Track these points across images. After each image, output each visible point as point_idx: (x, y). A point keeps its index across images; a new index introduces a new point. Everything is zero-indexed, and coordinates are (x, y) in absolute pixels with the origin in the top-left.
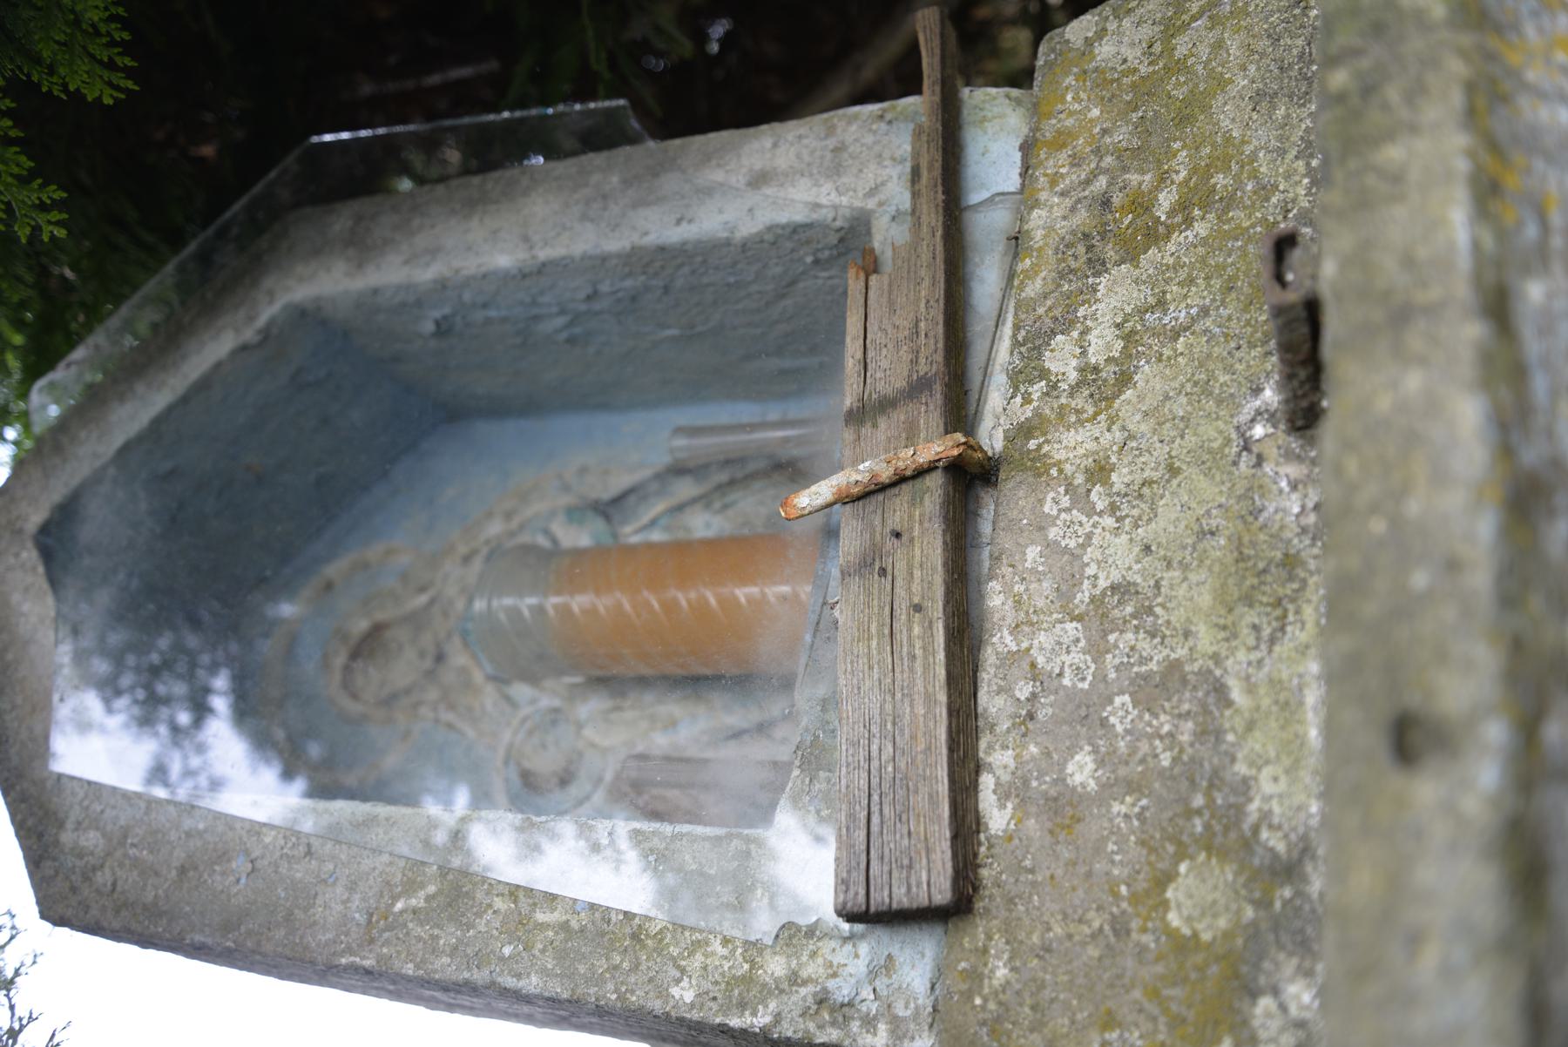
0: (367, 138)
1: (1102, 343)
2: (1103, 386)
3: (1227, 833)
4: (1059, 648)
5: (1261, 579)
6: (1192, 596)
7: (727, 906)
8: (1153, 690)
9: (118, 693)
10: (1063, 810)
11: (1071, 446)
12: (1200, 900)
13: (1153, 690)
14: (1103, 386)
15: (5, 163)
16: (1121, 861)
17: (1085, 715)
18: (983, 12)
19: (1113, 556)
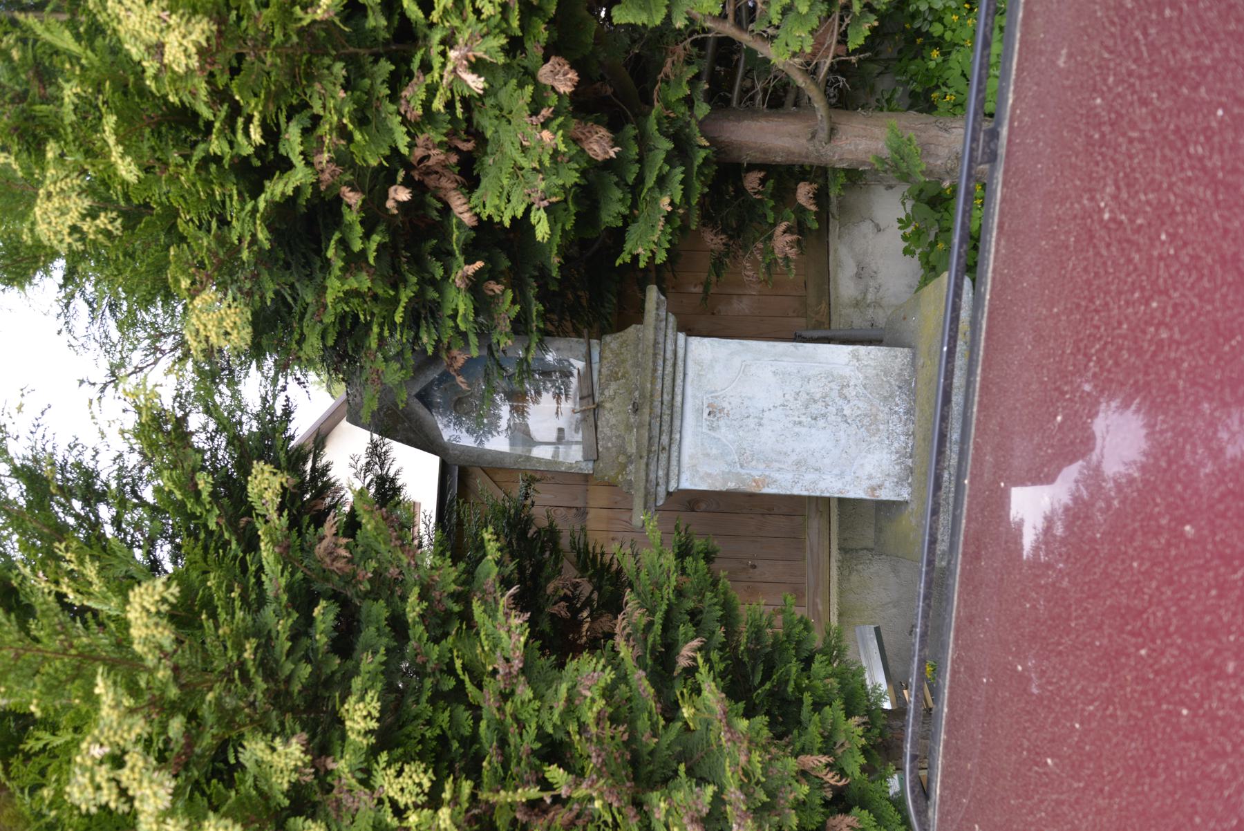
0: (1017, 16)
1: (612, 393)
2: (612, 399)
3: (625, 453)
4: (607, 430)
5: (629, 428)
6: (622, 427)
7: (627, 684)
8: (618, 437)
9: (122, 144)
10: (608, 449)
11: (608, 405)
12: (622, 459)
13: (618, 437)
14: (612, 399)
15: (1239, 706)
16: (614, 454)
17: (610, 439)
18: (904, 827)
19: (613, 421)
